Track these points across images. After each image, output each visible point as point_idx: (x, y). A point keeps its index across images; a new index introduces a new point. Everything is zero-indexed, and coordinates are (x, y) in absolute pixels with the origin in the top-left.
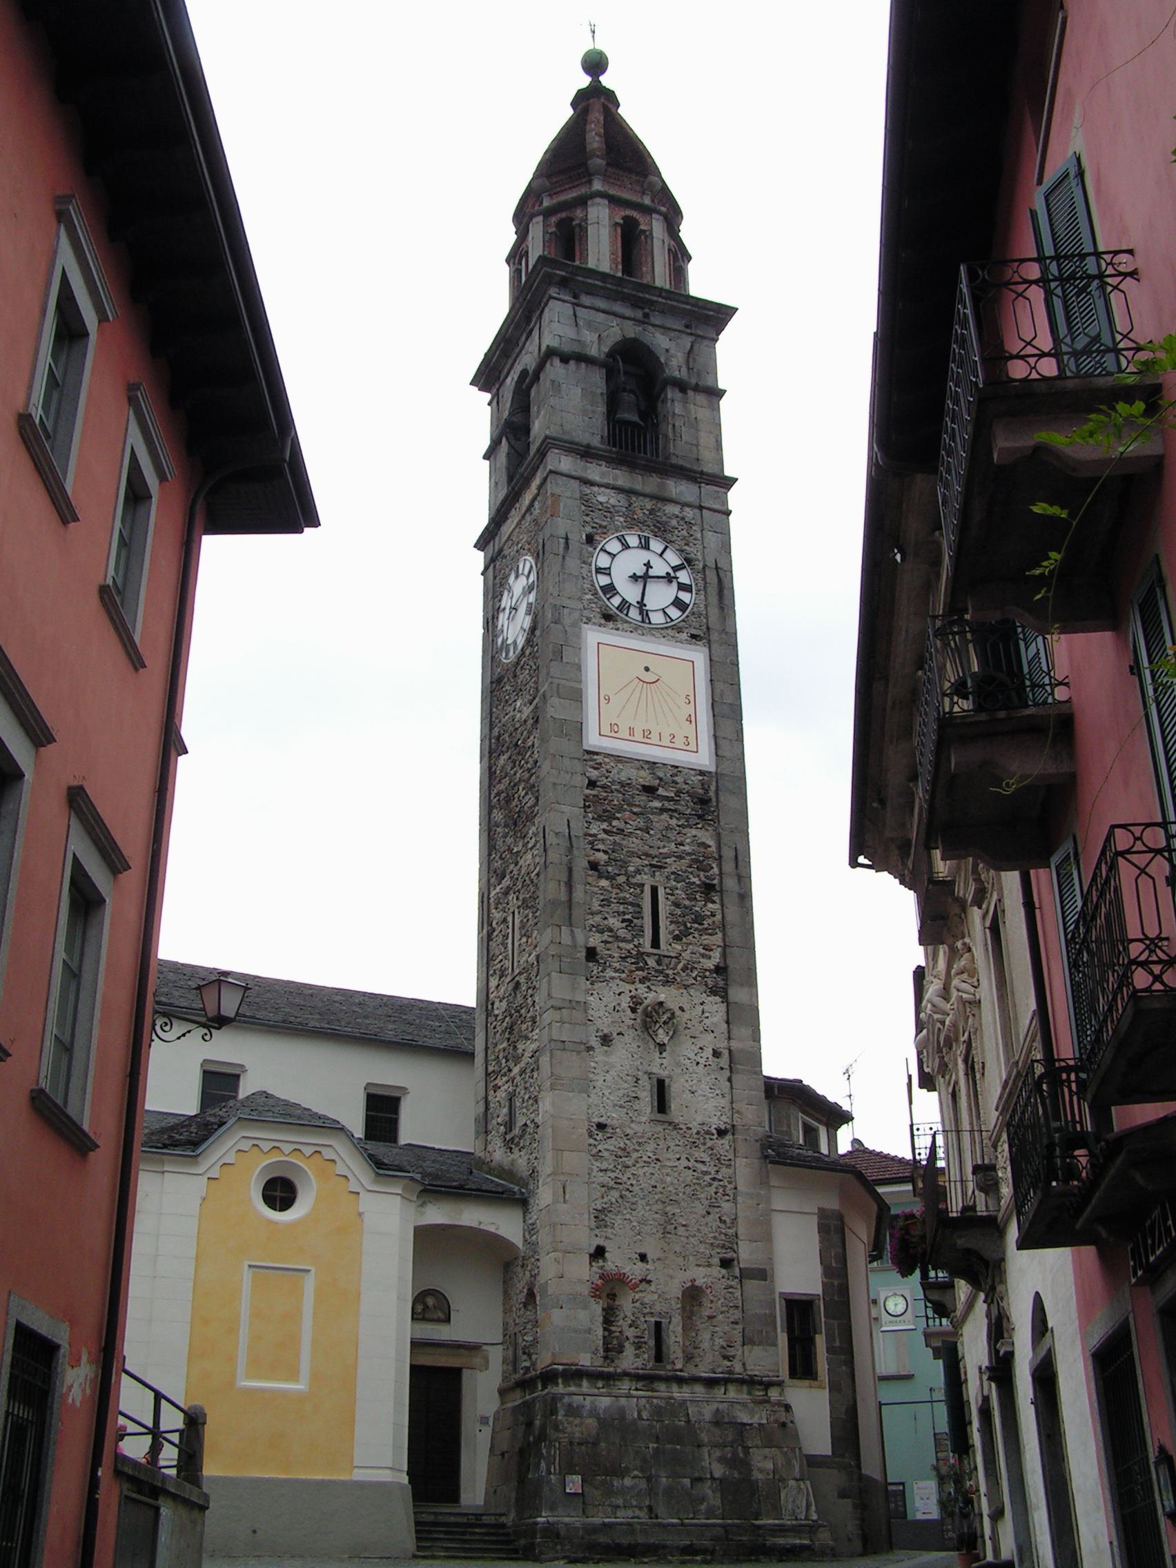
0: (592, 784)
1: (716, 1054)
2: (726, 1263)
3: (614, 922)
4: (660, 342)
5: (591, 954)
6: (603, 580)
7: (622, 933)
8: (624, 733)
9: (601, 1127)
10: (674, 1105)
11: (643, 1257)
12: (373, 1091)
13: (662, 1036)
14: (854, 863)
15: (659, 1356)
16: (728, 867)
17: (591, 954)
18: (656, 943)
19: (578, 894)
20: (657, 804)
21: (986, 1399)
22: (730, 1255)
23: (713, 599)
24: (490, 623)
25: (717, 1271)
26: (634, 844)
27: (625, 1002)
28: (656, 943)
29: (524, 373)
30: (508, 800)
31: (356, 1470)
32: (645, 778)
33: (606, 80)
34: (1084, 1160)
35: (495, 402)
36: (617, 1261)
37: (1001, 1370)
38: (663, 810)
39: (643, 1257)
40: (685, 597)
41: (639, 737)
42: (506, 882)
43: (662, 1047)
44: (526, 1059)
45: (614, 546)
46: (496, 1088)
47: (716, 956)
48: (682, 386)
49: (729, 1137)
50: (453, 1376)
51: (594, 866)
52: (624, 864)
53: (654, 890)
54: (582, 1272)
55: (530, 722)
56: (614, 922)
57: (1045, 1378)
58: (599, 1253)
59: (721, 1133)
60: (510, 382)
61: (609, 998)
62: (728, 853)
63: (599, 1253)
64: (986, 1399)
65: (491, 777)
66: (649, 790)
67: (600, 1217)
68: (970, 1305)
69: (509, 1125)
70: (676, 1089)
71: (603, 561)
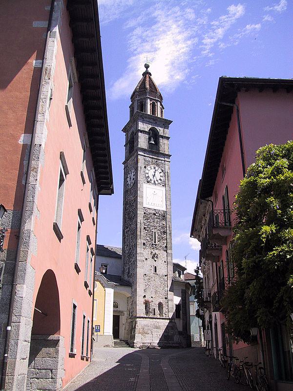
0: (145, 213)
1: (165, 262)
2: (166, 298)
3: (148, 238)
4: (158, 128)
5: (144, 244)
6: (147, 175)
8: (150, 204)
9: (145, 274)
10: (157, 271)
11: (152, 297)
12: (110, 191)
13: (156, 259)
14: (191, 237)
15: (154, 315)
16: (168, 228)
17: (144, 244)
18: (155, 242)
19: (142, 234)
21: (208, 325)
23: (167, 178)
24: (125, 179)
25: (164, 300)
26: (152, 224)
27: (150, 253)
28: (155, 242)
29: (133, 132)
30: (129, 214)
31: (147, 130)
32: (154, 212)
33: (149, 70)
34: (211, 63)
35: (127, 135)
36: (148, 298)
37: (210, 322)
39: (152, 297)
40: (161, 178)
41: (153, 204)
42: (128, 229)
43: (155, 261)
44: (132, 262)
45: (149, 169)
46: (126, 266)
47: (165, 245)
48: (162, 137)
50: (118, 317)
51: (145, 228)
52: (150, 228)
54: (143, 300)
56: (148, 238)
57: (216, 325)
58: (145, 296)
59: (165, 276)
60: (130, 132)
61: (147, 252)
62: (168, 226)
63: (145, 296)
64: (208, 325)
65: (125, 209)
67: (145, 291)
68: (206, 311)
69: (129, 273)
70: (157, 268)
71: (147, 172)
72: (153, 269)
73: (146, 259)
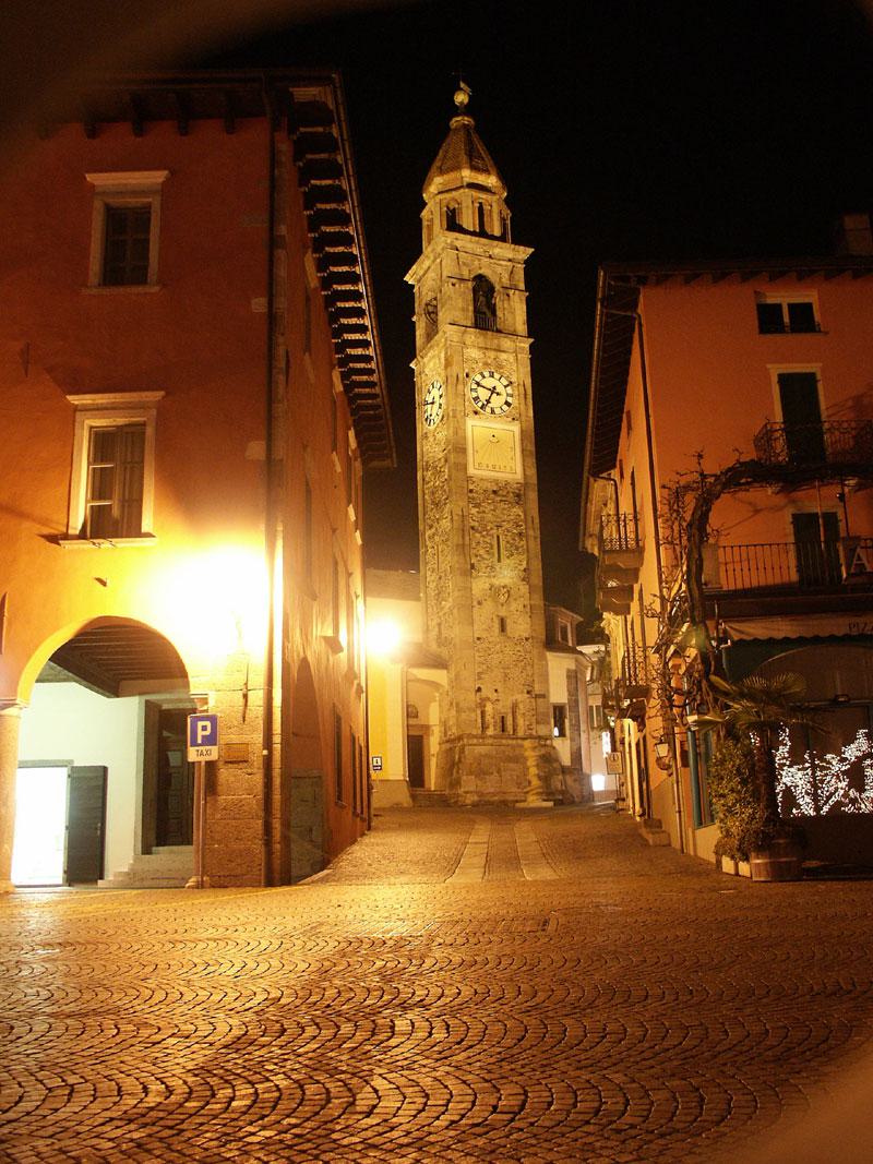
7: (485, 556)
9: (479, 639)
20: (499, 499)
22: (530, 689)
38: (501, 501)
49: (530, 640)
53: (498, 537)
55: (443, 460)
58: (479, 690)
63: (479, 690)
66: (495, 492)
72: (497, 626)
73: (479, 603)
